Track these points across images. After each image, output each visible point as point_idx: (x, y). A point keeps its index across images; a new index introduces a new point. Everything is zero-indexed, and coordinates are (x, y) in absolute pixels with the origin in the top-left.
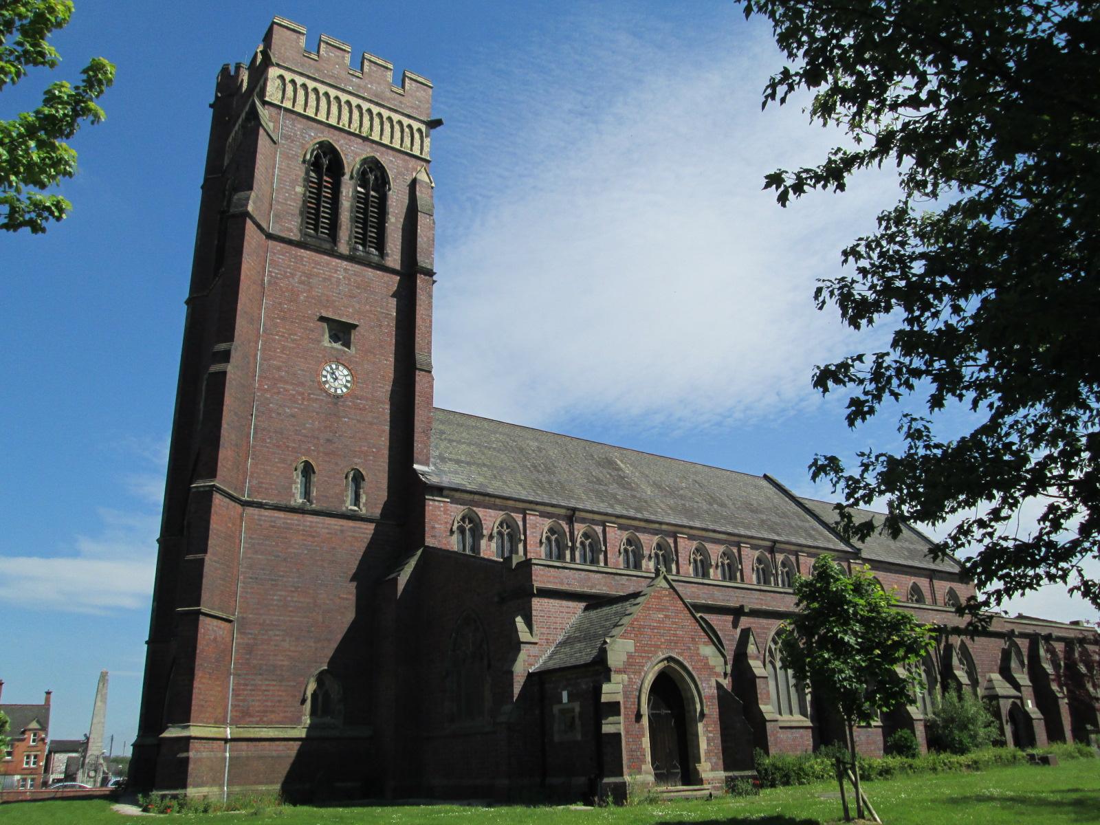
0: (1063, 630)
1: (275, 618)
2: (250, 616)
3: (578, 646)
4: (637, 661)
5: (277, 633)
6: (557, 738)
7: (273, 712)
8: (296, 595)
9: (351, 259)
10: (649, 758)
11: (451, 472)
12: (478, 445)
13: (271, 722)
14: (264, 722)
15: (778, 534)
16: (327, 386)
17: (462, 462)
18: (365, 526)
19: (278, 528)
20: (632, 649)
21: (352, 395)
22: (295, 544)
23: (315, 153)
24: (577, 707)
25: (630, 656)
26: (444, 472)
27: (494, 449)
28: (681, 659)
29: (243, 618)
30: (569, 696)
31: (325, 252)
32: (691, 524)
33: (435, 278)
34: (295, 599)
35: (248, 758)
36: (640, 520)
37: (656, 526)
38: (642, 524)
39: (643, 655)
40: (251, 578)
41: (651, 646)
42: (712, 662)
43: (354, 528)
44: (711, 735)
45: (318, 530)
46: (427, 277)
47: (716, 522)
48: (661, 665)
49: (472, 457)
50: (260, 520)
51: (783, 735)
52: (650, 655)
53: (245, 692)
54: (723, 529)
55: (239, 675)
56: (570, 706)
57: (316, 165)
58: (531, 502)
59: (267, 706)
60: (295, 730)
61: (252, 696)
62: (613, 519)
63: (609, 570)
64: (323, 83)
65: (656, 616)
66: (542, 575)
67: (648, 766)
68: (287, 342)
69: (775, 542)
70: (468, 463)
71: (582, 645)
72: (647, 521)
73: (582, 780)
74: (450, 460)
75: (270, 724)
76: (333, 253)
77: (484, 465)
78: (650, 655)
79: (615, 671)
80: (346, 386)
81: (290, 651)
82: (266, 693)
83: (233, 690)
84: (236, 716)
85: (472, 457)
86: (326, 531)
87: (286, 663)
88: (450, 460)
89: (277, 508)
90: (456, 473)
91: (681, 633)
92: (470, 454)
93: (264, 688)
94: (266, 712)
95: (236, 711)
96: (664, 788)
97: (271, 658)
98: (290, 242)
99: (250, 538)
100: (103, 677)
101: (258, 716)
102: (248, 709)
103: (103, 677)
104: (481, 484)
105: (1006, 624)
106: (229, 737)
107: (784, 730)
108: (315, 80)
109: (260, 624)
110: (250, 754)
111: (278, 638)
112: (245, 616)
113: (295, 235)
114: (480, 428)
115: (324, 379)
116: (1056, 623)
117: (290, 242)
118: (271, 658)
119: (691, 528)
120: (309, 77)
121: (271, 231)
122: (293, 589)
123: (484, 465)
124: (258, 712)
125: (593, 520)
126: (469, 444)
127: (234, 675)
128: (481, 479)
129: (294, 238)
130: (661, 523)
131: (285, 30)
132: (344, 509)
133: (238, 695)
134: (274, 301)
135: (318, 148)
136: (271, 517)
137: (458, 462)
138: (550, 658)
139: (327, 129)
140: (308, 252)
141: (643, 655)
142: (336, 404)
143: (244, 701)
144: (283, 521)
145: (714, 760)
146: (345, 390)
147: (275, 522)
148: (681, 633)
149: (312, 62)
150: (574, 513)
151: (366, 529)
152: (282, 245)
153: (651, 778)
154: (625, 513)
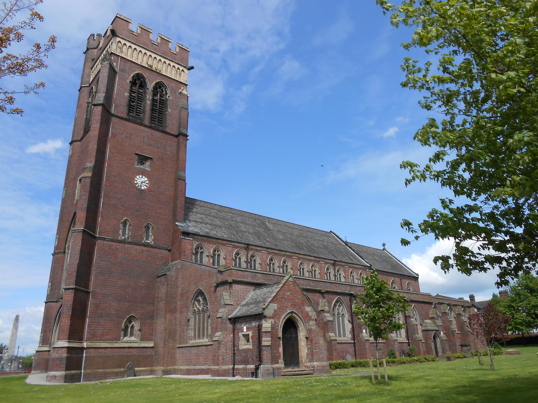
0: (456, 301)
1: (110, 291)
2: (97, 290)
3: (251, 306)
4: (278, 313)
5: (111, 298)
6: (241, 348)
7: (106, 335)
8: (120, 281)
9: (150, 127)
10: (282, 357)
11: (193, 227)
12: (205, 215)
13: (106, 340)
14: (103, 340)
15: (337, 258)
16: (137, 185)
17: (198, 222)
18: (153, 250)
19: (112, 250)
20: (276, 308)
21: (149, 189)
22: (120, 257)
23: (135, 78)
24: (250, 333)
25: (275, 311)
26: (190, 226)
27: (212, 216)
28: (297, 312)
29: (95, 291)
30: (247, 328)
31: (138, 124)
32: (299, 252)
33: (188, 138)
34: (119, 283)
35: (94, 356)
36: (277, 250)
37: (284, 253)
38: (278, 252)
39: (281, 310)
40: (99, 273)
41: (284, 307)
42: (310, 314)
43: (148, 250)
44: (309, 346)
45: (131, 251)
46: (185, 137)
47: (310, 252)
48: (289, 316)
49: (202, 220)
50: (103, 246)
51: (338, 346)
52: (284, 311)
53: (94, 326)
54: (313, 255)
55: (92, 318)
56: (247, 333)
57: (133, 83)
58: (229, 241)
59: (104, 332)
60: (117, 344)
61: (97, 327)
62: (265, 249)
63: (305, 278)
64: (139, 46)
65: (286, 293)
66: (235, 274)
67: (281, 360)
68: (119, 164)
69: (335, 261)
70: (201, 223)
71: (254, 306)
72: (280, 250)
73: (252, 366)
74: (193, 221)
75: (105, 340)
76: (141, 124)
77: (208, 224)
78: (284, 311)
79: (268, 318)
80: (146, 186)
81: (116, 307)
82: (104, 326)
83: (88, 325)
84: (90, 337)
85: (202, 220)
86: (135, 252)
87: (114, 312)
88: (193, 221)
89: (112, 241)
90: (195, 227)
91: (297, 301)
92: (202, 218)
93: (103, 324)
94: (103, 335)
95: (90, 335)
96: (290, 370)
97: (107, 310)
98: (122, 118)
99: (99, 254)
100: (17, 318)
101: (100, 337)
102: (95, 334)
103: (17, 318)
104: (207, 232)
105: (432, 299)
106: (85, 347)
107: (338, 344)
108: (135, 44)
109: (102, 294)
110: (95, 354)
111: (111, 301)
112: (95, 290)
113: (124, 115)
114: (206, 207)
115: (136, 182)
116: (452, 298)
117: (122, 118)
118: (107, 310)
119: (299, 254)
120: (133, 43)
121: (113, 113)
122: (119, 278)
123: (208, 224)
124: (100, 335)
125: (256, 249)
126: (201, 214)
127: (89, 317)
128: (207, 230)
129: (124, 117)
130: (286, 252)
131: (121, 20)
132: (143, 242)
133: (90, 327)
134: (113, 145)
135: (136, 76)
136: (109, 245)
137: (196, 222)
138: (238, 312)
139: (141, 67)
140: (130, 123)
141: (281, 310)
142: (141, 194)
143: (93, 330)
144: (115, 246)
145: (310, 357)
146: (145, 187)
147: (110, 247)
148: (297, 301)
149: (134, 36)
150: (335, 263)
151: (153, 251)
152: (118, 119)
153: (282, 366)
154: (270, 247)
